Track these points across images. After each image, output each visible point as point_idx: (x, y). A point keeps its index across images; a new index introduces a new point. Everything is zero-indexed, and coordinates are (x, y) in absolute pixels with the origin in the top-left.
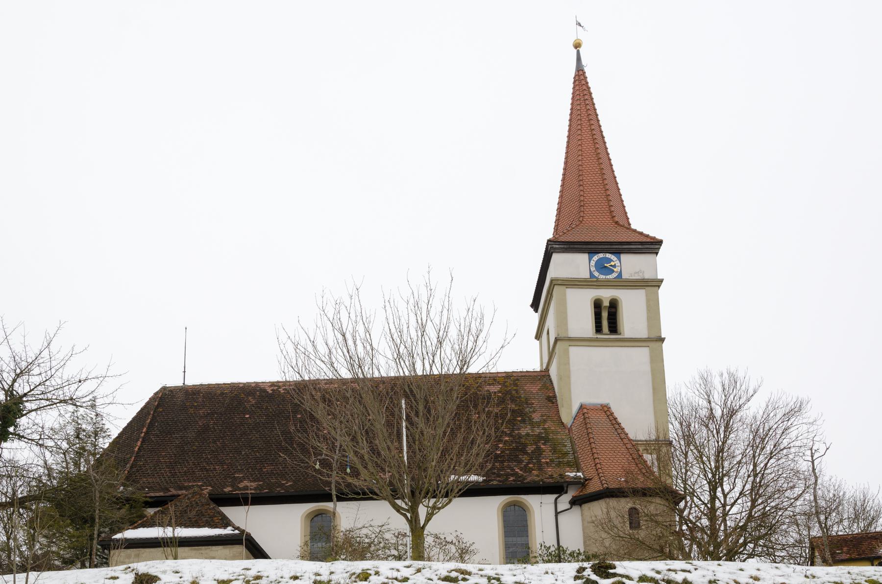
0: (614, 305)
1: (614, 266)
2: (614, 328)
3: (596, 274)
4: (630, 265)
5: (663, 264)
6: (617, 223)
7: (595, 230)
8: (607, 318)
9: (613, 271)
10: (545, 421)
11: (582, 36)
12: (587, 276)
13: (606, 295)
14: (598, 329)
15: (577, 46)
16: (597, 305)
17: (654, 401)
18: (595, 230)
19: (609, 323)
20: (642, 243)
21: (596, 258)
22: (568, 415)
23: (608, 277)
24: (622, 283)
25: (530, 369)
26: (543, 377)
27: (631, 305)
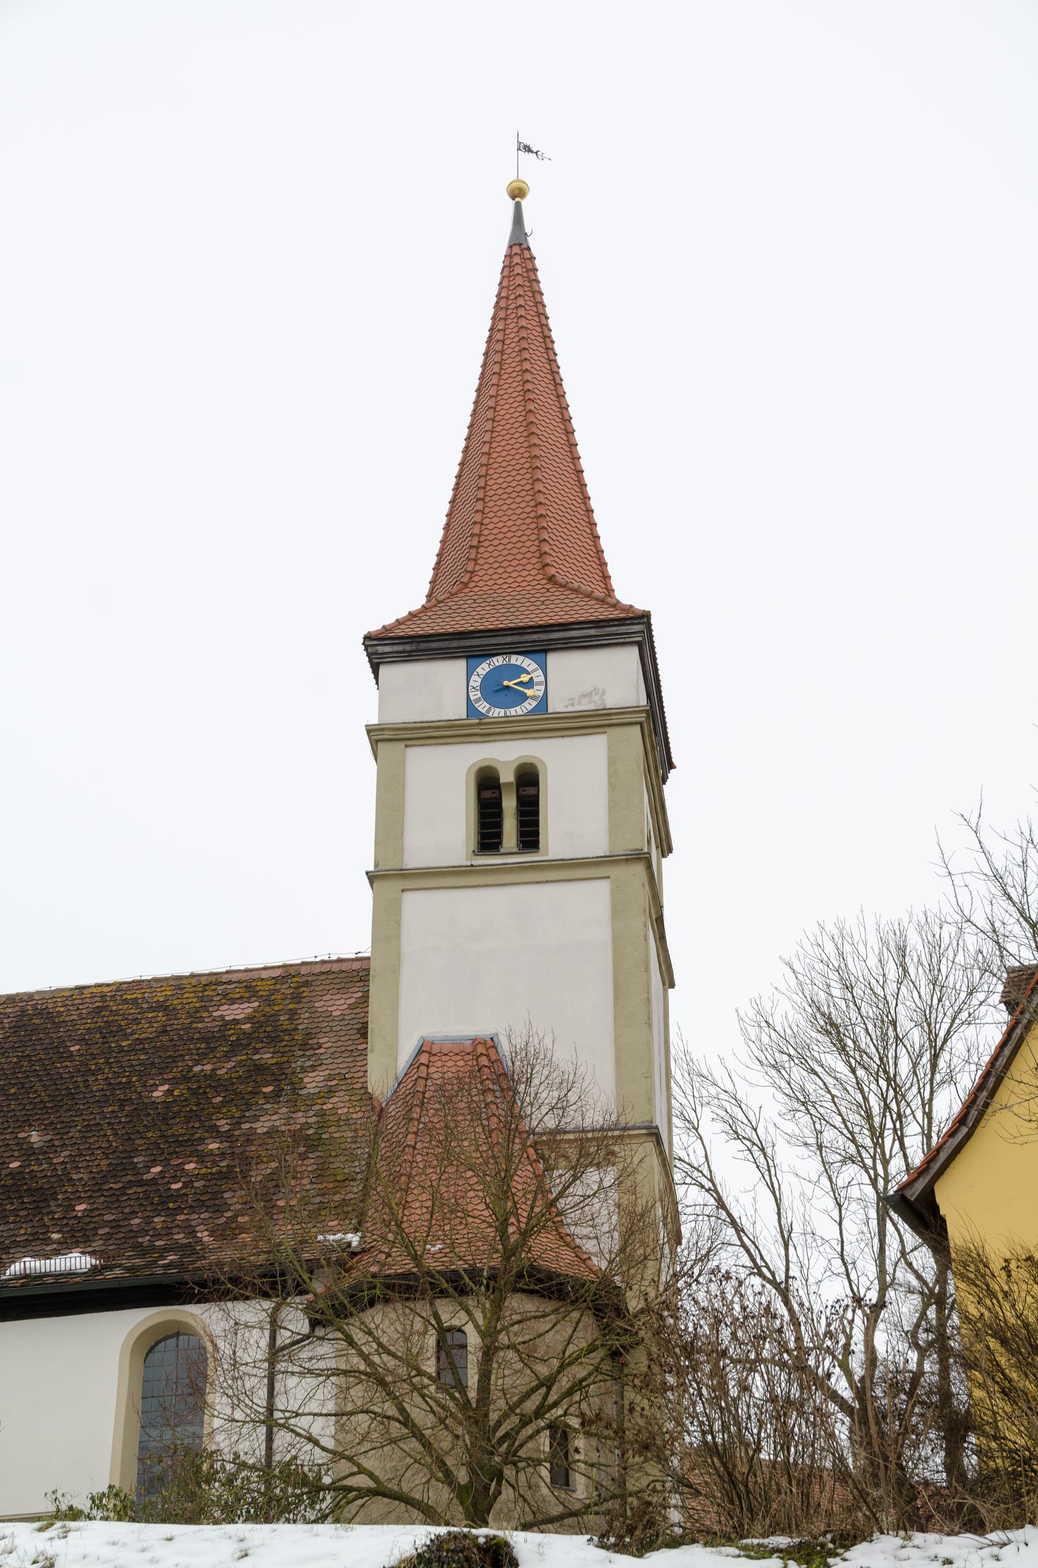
0: (528, 779)
1: (530, 684)
2: (530, 837)
3: (483, 707)
6: (551, 579)
7: (517, 601)
9: (525, 697)
10: (331, 1092)
11: (529, 170)
13: (505, 756)
14: (488, 839)
15: (517, 193)
16: (487, 783)
17: (616, 1018)
18: (517, 601)
20: (597, 624)
21: (484, 668)
22: (385, 1069)
23: (512, 711)
25: (602, 934)
26: (351, 976)
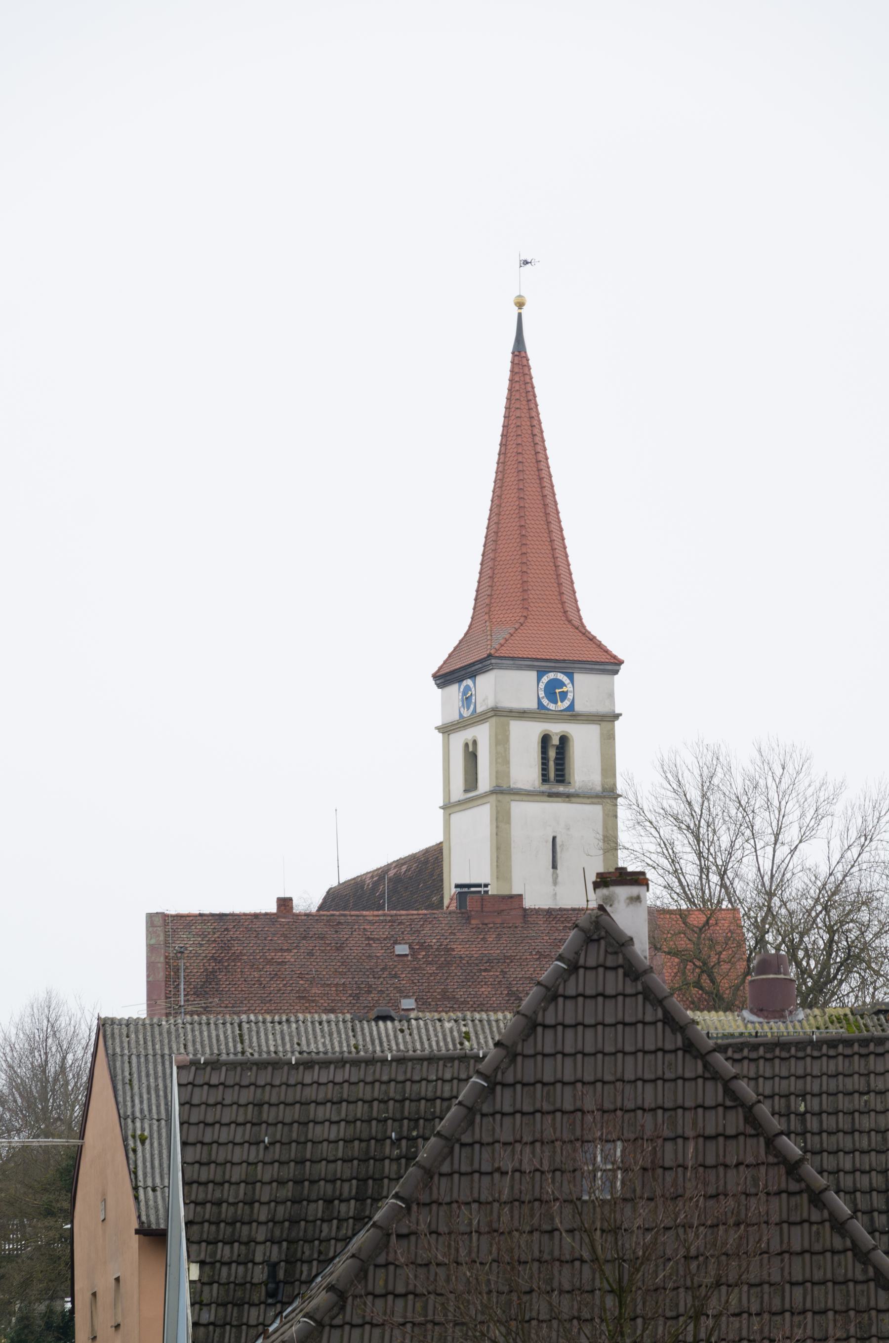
2: (562, 776)
3: (545, 702)
4: (584, 690)
5: (625, 690)
7: (527, 616)
8: (555, 759)
12: (577, 677)
13: (556, 729)
14: (545, 778)
15: (520, 305)
16: (545, 740)
19: (556, 764)
24: (572, 715)
27: (584, 740)
